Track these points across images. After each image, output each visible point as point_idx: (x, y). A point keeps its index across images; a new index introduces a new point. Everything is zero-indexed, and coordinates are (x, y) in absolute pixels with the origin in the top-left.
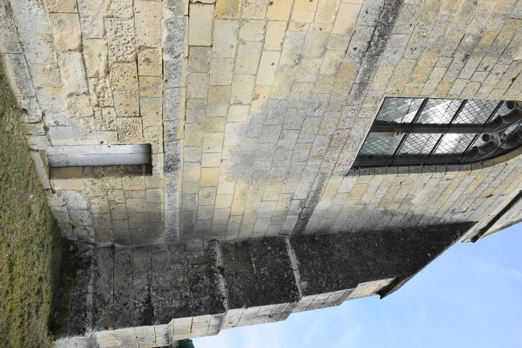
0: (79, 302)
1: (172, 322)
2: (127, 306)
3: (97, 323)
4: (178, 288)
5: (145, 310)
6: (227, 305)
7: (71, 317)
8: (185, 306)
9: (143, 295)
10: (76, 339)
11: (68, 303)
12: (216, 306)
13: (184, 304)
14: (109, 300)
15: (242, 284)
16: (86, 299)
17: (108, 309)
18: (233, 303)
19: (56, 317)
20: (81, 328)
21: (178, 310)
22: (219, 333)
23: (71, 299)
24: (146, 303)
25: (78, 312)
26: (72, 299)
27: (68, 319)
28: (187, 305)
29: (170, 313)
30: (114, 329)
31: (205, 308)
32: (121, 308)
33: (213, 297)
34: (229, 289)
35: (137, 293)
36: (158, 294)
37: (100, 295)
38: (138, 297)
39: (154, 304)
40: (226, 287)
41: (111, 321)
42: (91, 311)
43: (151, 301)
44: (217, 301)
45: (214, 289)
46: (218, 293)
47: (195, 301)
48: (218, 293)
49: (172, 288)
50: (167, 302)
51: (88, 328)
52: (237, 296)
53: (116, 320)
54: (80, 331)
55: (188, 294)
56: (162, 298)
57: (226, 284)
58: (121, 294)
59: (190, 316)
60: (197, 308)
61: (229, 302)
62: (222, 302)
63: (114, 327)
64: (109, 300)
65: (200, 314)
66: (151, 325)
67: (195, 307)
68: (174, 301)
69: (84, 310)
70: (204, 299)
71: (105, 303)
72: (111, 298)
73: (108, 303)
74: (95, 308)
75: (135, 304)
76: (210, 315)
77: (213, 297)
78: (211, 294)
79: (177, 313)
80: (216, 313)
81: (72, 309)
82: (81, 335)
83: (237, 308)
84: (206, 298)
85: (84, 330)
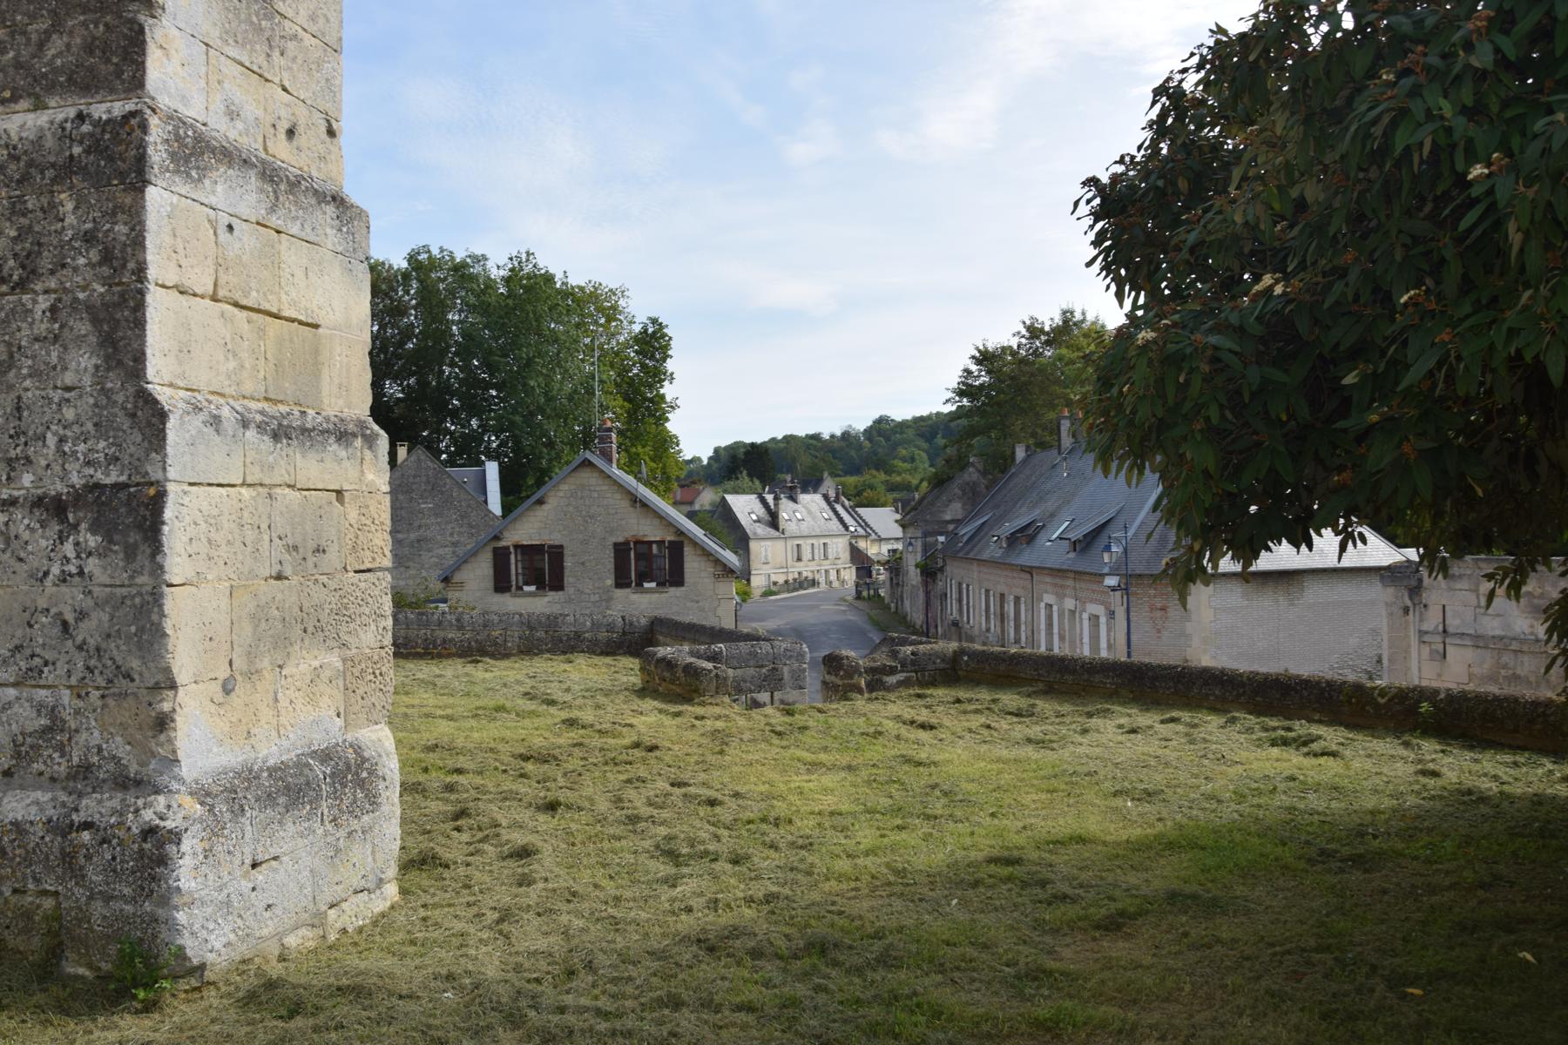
0: (27, 861)
1: (163, 394)
2: (70, 617)
3: (133, 769)
4: (11, 356)
5: (93, 530)
6: (118, 104)
7: (91, 898)
8: (95, 321)
9: (26, 535)
10: (188, 871)
11: (27, 915)
12: (111, 159)
13: (83, 327)
14: (40, 708)
15: (33, 17)
16: (15, 824)
17: (77, 712)
18: (119, 74)
19: (90, 966)
20: (141, 850)
21: (107, 358)
22: (354, 193)
23: (14, 899)
24: (63, 519)
25: (69, 862)
26: (15, 891)
27: (98, 908)
28: (89, 308)
29: (120, 398)
30: (173, 686)
31: (114, 214)
32: (80, 648)
33: (69, 168)
34: (51, 88)
35: (18, 566)
36: (29, 461)
37: (18, 755)
38: (34, 562)
39: (76, 479)
40: (39, 106)
41: (130, 699)
42: (80, 795)
43: (58, 497)
44: (87, 152)
45: (31, 164)
46: (49, 142)
47: (76, 269)
48: (49, 142)
49: (11, 387)
50: (69, 414)
51: (148, 815)
52: (89, 49)
53: (128, 676)
54: (153, 851)
55: (44, 303)
56: (51, 440)
57: (24, 104)
58: (18, 648)
59: (142, 293)
60: (107, 257)
61: (112, 91)
62: (98, 123)
63: (157, 687)
64: (40, 708)
65: (137, 241)
66: (161, 496)
67: (106, 271)
68: (69, 378)
69: (64, 836)
70: (71, 219)
71: (55, 728)
72: (30, 700)
73: (53, 712)
74: (71, 777)
75: (64, 578)
76: (152, 193)
77: (69, 168)
78: (54, 181)
79: (120, 363)
80: (141, 160)
81: (56, 893)
82: (171, 849)
83: (143, 53)
84: (70, 206)
85: (150, 832)
